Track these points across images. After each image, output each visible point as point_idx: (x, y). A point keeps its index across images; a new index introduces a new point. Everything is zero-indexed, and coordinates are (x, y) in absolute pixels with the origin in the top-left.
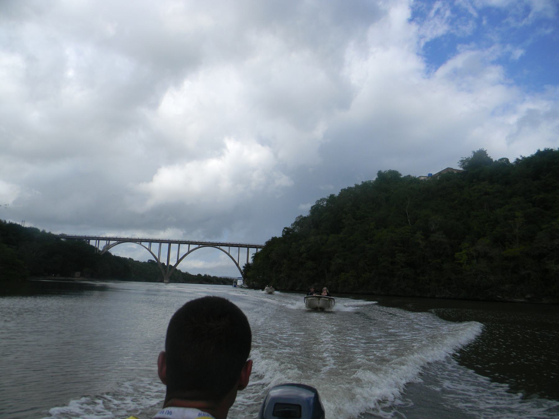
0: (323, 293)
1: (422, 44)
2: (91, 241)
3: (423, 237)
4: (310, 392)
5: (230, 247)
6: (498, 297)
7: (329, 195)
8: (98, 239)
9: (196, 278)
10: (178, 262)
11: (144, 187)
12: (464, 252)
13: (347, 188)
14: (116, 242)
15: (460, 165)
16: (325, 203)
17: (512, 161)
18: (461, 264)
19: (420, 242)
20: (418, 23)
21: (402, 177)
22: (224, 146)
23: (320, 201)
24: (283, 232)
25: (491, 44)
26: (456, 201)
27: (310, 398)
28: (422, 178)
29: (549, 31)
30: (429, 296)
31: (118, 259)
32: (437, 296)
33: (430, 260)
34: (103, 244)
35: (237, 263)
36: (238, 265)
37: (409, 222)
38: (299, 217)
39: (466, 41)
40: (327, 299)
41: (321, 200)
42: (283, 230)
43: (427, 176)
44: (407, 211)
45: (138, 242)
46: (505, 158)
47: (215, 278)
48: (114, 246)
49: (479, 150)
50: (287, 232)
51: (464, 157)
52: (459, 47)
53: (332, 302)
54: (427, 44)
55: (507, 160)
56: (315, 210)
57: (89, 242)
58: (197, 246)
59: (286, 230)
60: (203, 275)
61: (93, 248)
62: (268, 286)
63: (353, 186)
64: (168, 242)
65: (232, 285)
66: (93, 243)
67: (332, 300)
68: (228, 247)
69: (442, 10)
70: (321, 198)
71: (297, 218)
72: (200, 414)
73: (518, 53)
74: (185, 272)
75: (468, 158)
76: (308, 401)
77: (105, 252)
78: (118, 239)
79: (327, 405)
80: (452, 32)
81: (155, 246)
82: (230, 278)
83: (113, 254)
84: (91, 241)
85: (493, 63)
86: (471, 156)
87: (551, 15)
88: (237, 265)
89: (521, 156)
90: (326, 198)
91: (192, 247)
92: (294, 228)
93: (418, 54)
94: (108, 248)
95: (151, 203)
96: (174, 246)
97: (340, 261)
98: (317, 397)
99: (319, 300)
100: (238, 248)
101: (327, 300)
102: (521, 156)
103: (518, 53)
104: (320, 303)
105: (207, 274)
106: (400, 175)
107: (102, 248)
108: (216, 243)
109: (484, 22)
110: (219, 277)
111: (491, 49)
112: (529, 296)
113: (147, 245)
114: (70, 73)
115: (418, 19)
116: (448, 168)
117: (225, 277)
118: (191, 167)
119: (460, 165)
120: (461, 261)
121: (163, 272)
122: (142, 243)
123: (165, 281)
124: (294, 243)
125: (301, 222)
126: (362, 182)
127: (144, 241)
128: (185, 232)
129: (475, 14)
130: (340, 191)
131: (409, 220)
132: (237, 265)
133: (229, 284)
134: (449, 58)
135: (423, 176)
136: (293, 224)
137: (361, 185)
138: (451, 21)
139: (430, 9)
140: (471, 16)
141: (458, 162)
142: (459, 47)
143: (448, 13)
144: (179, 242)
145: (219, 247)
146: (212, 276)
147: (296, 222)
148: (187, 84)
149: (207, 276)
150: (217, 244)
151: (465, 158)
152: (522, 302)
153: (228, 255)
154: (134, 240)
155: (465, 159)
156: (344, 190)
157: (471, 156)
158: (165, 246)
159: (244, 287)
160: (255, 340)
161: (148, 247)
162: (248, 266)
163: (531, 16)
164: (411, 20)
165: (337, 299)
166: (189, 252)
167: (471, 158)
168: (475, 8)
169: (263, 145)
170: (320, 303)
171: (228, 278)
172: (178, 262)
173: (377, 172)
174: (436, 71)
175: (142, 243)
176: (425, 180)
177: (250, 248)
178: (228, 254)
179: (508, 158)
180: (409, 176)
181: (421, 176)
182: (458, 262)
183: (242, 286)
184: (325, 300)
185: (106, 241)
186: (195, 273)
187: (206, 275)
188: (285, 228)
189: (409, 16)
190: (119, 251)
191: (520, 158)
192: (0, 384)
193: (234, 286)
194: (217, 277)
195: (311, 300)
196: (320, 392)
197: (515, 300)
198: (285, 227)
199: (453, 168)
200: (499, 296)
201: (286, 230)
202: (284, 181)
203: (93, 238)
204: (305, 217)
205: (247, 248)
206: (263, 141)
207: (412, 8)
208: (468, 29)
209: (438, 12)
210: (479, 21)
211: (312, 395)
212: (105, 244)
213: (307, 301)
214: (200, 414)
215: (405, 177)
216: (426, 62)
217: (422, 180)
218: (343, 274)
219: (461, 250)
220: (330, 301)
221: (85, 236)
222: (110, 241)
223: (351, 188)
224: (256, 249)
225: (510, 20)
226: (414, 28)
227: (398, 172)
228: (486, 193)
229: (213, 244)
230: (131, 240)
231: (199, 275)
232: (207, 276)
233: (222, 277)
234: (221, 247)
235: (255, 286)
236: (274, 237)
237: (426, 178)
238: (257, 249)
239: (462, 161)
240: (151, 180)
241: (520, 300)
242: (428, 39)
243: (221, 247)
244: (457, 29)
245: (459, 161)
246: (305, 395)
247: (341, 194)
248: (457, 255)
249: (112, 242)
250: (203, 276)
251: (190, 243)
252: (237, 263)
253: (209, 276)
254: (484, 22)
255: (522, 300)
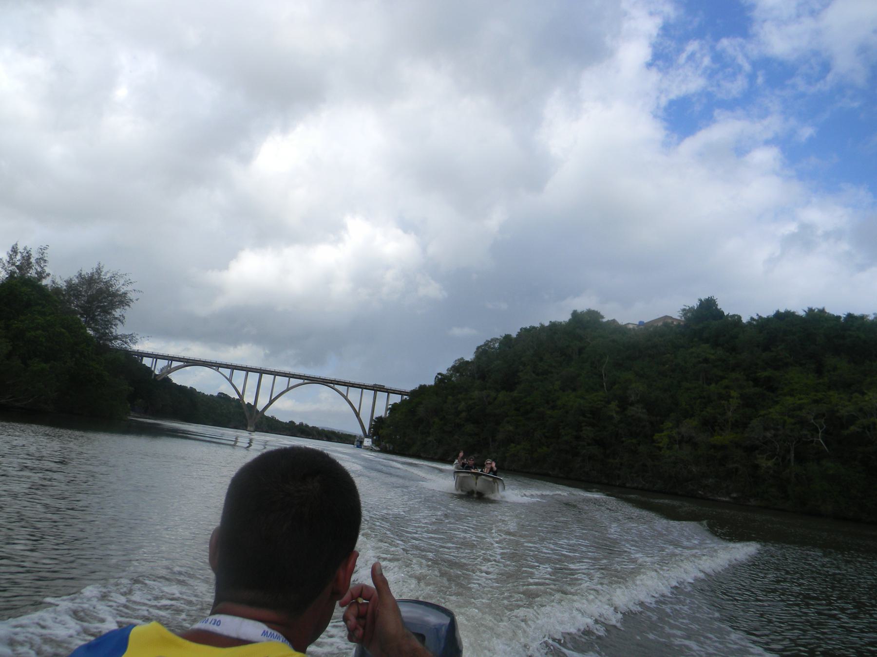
0: (486, 469)
1: (664, 101)
2: (144, 358)
3: (618, 409)
4: (444, 616)
5: (350, 388)
6: (699, 493)
7: (504, 335)
8: (156, 357)
9: (287, 426)
10: (271, 402)
11: (213, 277)
12: (665, 433)
13: (528, 327)
14: (182, 363)
15: (681, 315)
16: (497, 345)
17: (745, 320)
18: (660, 449)
19: (615, 415)
20: (660, 70)
21: (605, 320)
22: (344, 227)
23: (491, 342)
24: (435, 379)
25: (765, 113)
26: (667, 366)
27: (441, 625)
28: (631, 326)
29: (856, 105)
30: (618, 484)
31: (182, 389)
32: (628, 485)
33: (624, 439)
34: (162, 364)
35: (241, 394)
36: (359, 415)
37: (605, 386)
38: (459, 360)
39: (731, 105)
40: (491, 479)
41: (492, 340)
42: (436, 376)
43: (638, 323)
44: (603, 372)
45: (215, 367)
46: (737, 315)
47: (314, 428)
48: (176, 370)
49: (707, 298)
50: (441, 380)
51: (687, 305)
52: (717, 112)
53: (498, 485)
54: (672, 103)
55: (740, 317)
56: (483, 352)
57: (142, 360)
58: (301, 381)
59: (440, 377)
60: (297, 423)
61: (149, 371)
62: (376, 440)
63: (537, 325)
64: (259, 371)
65: (353, 444)
66: (147, 362)
67: (498, 481)
68: (347, 387)
69: (698, 55)
70: (493, 338)
71: (456, 361)
72: (272, 633)
73: (807, 132)
74: (270, 416)
75: (691, 307)
76: (437, 629)
77: (164, 376)
78: (186, 360)
79: (465, 638)
80: (710, 89)
81: (239, 375)
82: (337, 432)
83: (174, 381)
84: (144, 358)
85: (767, 143)
86: (697, 304)
87: (860, 79)
88: (357, 415)
89: (758, 315)
90: (499, 337)
91: (294, 381)
92: (451, 375)
93: (655, 117)
94: (169, 372)
95: (220, 303)
96: (267, 379)
97: (511, 428)
98: (452, 627)
99: (477, 478)
100: (361, 389)
101: (489, 481)
102: (758, 315)
103: (807, 132)
104: (478, 485)
105: (304, 423)
106: (602, 317)
107: (158, 370)
108: (330, 380)
109: (760, 80)
110: (320, 429)
111: (766, 122)
112: (735, 495)
113: (227, 372)
114: (121, 93)
115: (660, 63)
116: (666, 316)
117: (330, 430)
118: (291, 253)
119: (681, 315)
120: (661, 445)
121: (247, 414)
122: (220, 368)
123: (249, 428)
124: (450, 397)
125: (460, 367)
126: (550, 322)
127: (224, 366)
128: (267, 352)
129: (747, 67)
130: (519, 331)
131: (604, 384)
132: (357, 415)
133: (336, 440)
134: (700, 129)
135: (631, 324)
136: (449, 369)
137: (547, 326)
138: (711, 75)
139: (680, 51)
140: (740, 68)
141: (679, 311)
142: (717, 112)
143: (707, 61)
144: (275, 373)
145: (332, 385)
146: (311, 425)
147: (453, 367)
148: (300, 128)
149: (304, 425)
150: (330, 382)
151: (689, 306)
152: (726, 502)
153: (345, 399)
154: (209, 364)
155: (687, 308)
156: (525, 329)
157: (697, 304)
158: (253, 377)
159: (375, 450)
160: (364, 527)
161: (229, 378)
162: (380, 419)
163: (830, 77)
164: (649, 65)
165: (507, 481)
166: (288, 389)
167: (696, 307)
168: (747, 57)
169: (405, 231)
170: (477, 484)
171: (335, 431)
172: (271, 402)
173: (572, 312)
174: (678, 144)
175: (220, 368)
176: (634, 329)
177: (378, 392)
178: (346, 398)
179: (741, 315)
180: (614, 321)
181: (629, 324)
182: (657, 445)
183: (372, 448)
184: (485, 479)
185: (167, 361)
186: (285, 419)
187: (301, 424)
188: (439, 374)
189: (649, 58)
190: (181, 378)
191: (756, 317)
192: (1, 558)
193: (356, 446)
194: (317, 428)
195: (464, 477)
196: (460, 619)
197: (719, 498)
198: (439, 372)
199: (673, 317)
200: (700, 492)
201: (440, 377)
202: (432, 290)
203: (148, 355)
204: (467, 362)
205: (374, 391)
206: (407, 226)
207: (654, 46)
208: (736, 87)
209: (691, 57)
210: (752, 77)
211: (446, 621)
212: (167, 364)
213: (458, 478)
214: (272, 633)
215: (608, 321)
216: (667, 129)
217: (630, 329)
218: (513, 445)
219: (662, 431)
220: (494, 484)
221: (138, 350)
222: (173, 362)
223: (534, 328)
224: (387, 394)
225: (800, 82)
226: (654, 76)
227: (599, 313)
228: (706, 360)
229: (326, 381)
230: (206, 363)
231: (292, 423)
232: (304, 425)
233: (326, 429)
234: (336, 387)
235: (388, 449)
236: (423, 384)
237: (636, 326)
238: (348, 388)
239: (684, 310)
240: (225, 267)
241: (724, 499)
242: (672, 96)
243: (335, 386)
244: (719, 86)
245: (680, 310)
246: (434, 619)
247: (519, 335)
248: (657, 436)
249: (175, 364)
250: (298, 425)
251: (291, 376)
252: (358, 411)
253: (307, 426)
254: (760, 80)
255: (727, 499)
